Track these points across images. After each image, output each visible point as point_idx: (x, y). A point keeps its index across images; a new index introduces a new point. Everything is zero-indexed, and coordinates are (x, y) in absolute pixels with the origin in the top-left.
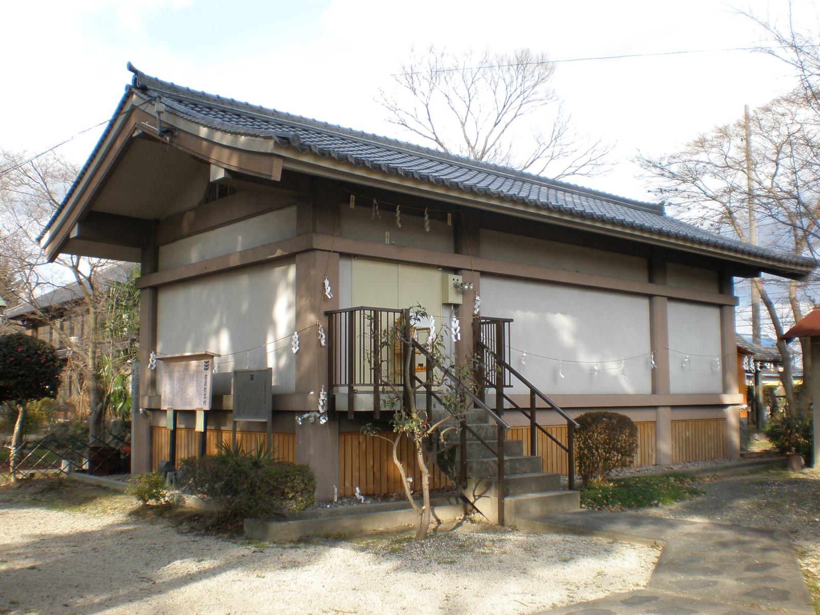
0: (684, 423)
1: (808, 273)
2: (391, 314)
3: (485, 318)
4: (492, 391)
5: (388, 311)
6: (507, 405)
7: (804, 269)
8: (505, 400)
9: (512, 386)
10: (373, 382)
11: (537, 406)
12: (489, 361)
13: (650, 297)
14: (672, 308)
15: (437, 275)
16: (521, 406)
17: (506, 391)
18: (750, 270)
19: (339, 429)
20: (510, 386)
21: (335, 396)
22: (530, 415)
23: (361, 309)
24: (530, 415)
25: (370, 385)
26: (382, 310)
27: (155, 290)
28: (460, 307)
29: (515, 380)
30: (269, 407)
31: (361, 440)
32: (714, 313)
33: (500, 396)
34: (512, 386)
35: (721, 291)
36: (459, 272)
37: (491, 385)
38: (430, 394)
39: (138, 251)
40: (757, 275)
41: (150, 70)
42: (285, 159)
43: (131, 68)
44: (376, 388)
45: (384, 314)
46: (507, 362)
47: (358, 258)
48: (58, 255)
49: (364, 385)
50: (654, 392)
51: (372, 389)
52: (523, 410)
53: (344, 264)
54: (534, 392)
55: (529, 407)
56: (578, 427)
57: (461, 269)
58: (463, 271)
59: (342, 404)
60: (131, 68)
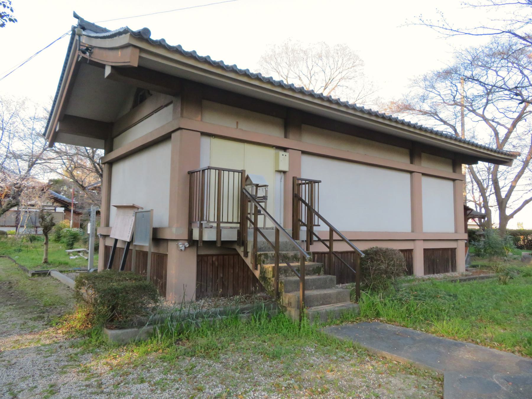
0: (217, 171)
1: (511, 160)
2: (231, 173)
3: (306, 180)
4: (304, 229)
5: (229, 170)
6: (315, 238)
7: (509, 157)
8: (314, 236)
9: (319, 226)
10: (216, 220)
11: (334, 239)
12: (304, 208)
13: (411, 172)
14: (425, 180)
15: (272, 152)
16: (322, 238)
17: (315, 229)
18: (472, 159)
19: (197, 253)
20: (318, 225)
21: (192, 229)
22: (329, 245)
23: (209, 168)
24: (329, 245)
25: (237, 223)
26: (224, 170)
27: (111, 164)
28: (287, 173)
29: (321, 222)
30: (150, 235)
31: (214, 259)
32: (449, 185)
33: (310, 233)
34: (319, 226)
35: (454, 171)
36: (288, 150)
37: (304, 225)
38: (257, 229)
39: (102, 142)
40: (476, 163)
41: (89, 18)
42: (141, 50)
43: (76, 16)
44: (218, 225)
45: (226, 173)
46: (316, 210)
47: (215, 138)
48: (54, 144)
49: (228, 222)
50: (413, 231)
51: (215, 225)
52: (323, 241)
53: (206, 141)
54: (332, 230)
55: (329, 239)
56: (364, 257)
57: (288, 148)
58: (290, 150)
59: (196, 236)
60: (76, 16)
